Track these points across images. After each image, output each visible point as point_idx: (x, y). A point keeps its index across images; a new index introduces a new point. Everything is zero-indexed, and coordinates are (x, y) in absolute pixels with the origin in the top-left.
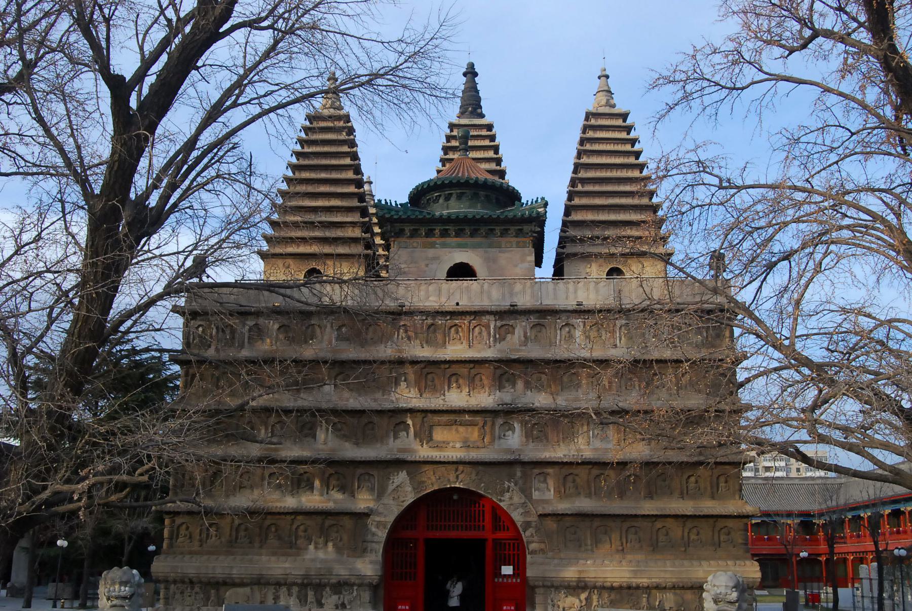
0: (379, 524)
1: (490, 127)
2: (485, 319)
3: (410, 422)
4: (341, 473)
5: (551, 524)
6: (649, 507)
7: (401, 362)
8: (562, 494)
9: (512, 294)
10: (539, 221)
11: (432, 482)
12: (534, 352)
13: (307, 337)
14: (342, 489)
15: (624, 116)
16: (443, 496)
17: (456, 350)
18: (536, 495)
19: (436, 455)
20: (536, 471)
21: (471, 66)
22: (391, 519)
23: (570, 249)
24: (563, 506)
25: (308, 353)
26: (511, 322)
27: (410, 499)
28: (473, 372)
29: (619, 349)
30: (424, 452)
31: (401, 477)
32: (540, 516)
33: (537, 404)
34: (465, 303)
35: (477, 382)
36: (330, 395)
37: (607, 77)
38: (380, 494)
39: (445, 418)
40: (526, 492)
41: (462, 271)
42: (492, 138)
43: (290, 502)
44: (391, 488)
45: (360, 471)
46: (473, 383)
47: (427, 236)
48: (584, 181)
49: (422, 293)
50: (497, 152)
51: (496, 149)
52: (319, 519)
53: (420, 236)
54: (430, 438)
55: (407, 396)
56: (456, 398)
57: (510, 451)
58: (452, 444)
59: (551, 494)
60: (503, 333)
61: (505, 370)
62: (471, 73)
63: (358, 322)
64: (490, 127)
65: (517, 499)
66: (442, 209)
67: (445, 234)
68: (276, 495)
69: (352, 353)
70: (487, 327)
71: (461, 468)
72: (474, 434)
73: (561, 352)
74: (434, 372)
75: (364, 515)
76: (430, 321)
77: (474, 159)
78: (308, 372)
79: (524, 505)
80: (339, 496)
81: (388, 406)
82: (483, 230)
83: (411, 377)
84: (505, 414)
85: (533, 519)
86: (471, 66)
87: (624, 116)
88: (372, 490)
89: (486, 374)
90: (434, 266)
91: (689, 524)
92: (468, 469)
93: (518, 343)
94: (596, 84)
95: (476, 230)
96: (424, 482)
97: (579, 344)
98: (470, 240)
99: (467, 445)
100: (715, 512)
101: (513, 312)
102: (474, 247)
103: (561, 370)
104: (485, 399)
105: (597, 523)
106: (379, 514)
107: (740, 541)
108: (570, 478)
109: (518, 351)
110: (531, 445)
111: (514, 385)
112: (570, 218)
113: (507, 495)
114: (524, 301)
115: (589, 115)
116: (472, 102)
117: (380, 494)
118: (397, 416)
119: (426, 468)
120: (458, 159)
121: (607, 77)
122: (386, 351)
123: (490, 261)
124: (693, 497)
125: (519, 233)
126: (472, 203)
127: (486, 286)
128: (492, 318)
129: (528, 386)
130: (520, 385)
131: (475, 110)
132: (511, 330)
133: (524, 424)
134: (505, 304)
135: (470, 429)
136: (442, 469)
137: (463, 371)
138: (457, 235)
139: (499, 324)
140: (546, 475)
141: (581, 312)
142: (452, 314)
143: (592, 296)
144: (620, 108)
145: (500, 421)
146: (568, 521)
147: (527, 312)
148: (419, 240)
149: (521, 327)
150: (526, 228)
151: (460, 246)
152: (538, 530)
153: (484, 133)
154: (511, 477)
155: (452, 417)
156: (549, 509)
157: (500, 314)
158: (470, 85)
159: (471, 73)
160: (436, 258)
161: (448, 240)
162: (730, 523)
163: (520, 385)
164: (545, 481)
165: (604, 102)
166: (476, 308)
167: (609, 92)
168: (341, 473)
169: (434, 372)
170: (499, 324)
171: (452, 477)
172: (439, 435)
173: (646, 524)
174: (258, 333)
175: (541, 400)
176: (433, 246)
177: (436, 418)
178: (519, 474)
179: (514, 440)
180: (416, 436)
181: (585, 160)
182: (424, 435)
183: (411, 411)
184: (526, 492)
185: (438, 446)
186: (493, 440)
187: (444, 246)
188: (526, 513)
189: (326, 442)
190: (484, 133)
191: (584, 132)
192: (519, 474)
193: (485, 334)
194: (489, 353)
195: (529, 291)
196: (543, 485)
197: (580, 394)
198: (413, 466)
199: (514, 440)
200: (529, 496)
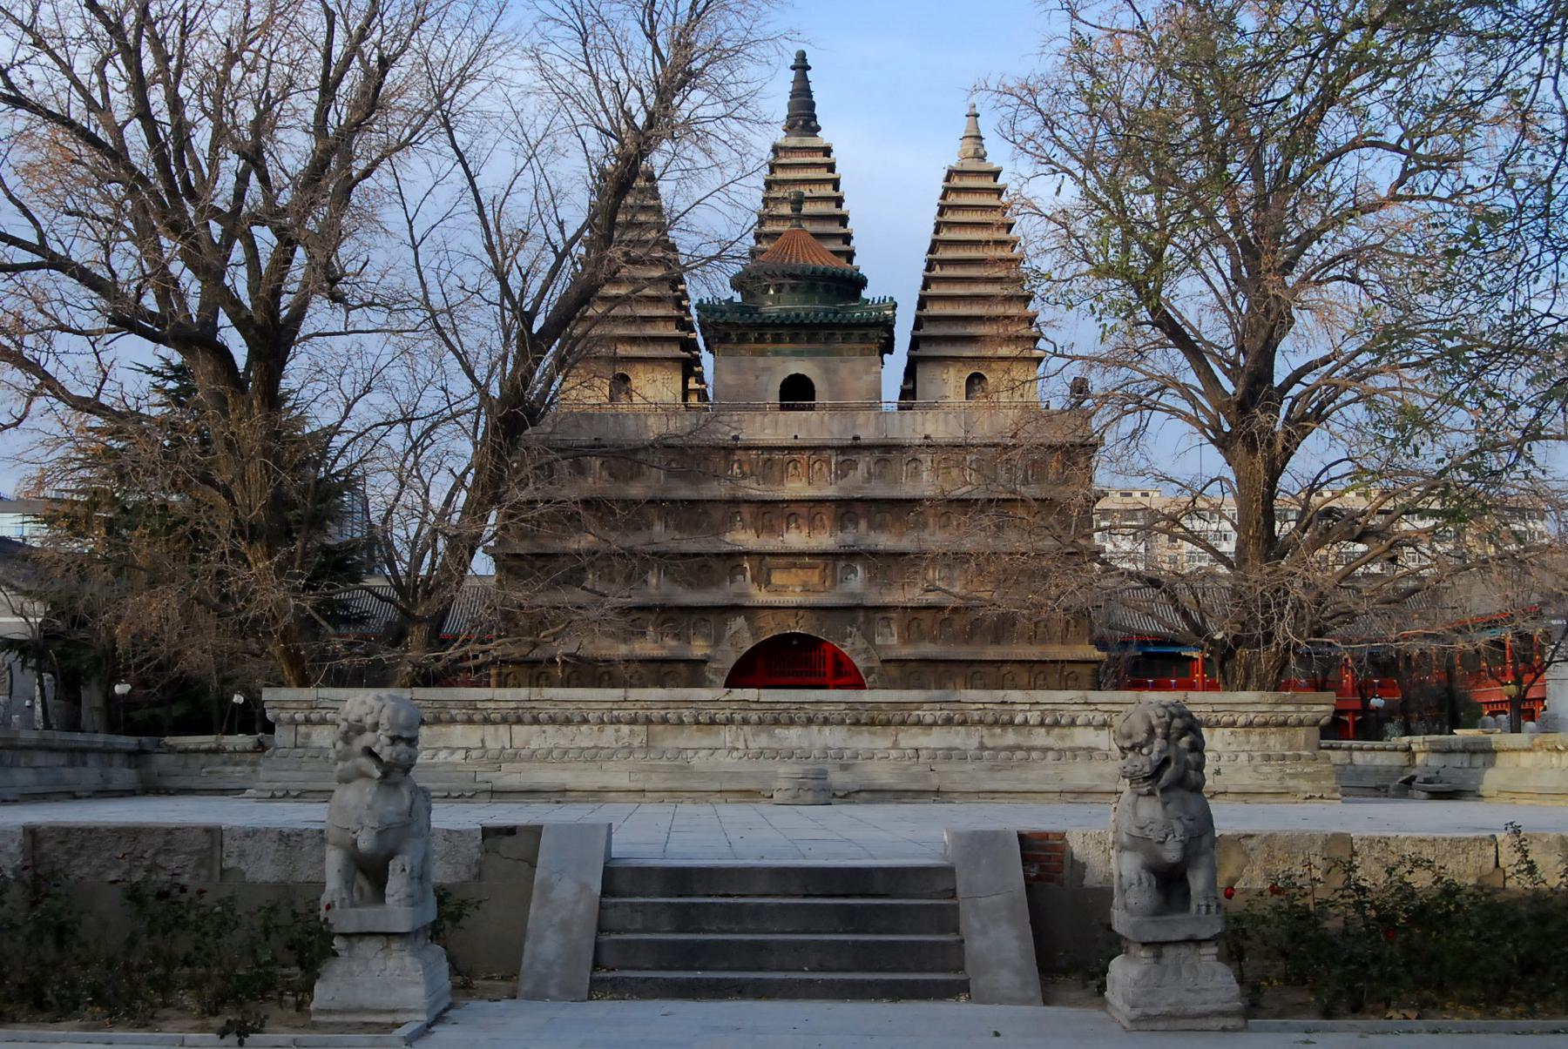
0: (717, 672)
1: (827, 151)
2: (826, 454)
3: (747, 565)
4: (672, 616)
5: (893, 670)
6: (992, 653)
7: (734, 502)
8: (906, 640)
9: (854, 426)
10: (888, 325)
11: (771, 628)
12: (879, 490)
13: (636, 475)
14: (677, 636)
15: (996, 174)
16: (783, 641)
17: (795, 488)
18: (878, 640)
19: (774, 599)
20: (879, 615)
21: (802, 56)
22: (730, 665)
23: (925, 350)
24: (907, 652)
25: (636, 490)
26: (854, 457)
27: (748, 645)
28: (814, 511)
29: (964, 484)
30: (761, 597)
31: (739, 622)
32: (884, 661)
33: (881, 547)
34: (804, 437)
35: (818, 522)
36: (662, 535)
37: (977, 116)
38: (717, 641)
39: (782, 561)
40: (868, 637)
41: (797, 392)
42: (831, 167)
43: (622, 650)
44: (728, 634)
45: (695, 617)
46: (812, 524)
47: (757, 341)
48: (943, 263)
49: (757, 425)
50: (836, 188)
51: (836, 184)
52: (653, 666)
53: (748, 341)
54: (768, 583)
55: (744, 538)
56: (796, 539)
57: (852, 595)
58: (791, 589)
59: (894, 640)
60: (845, 469)
61: (846, 509)
62: (801, 66)
63: (690, 456)
64: (827, 151)
65: (861, 644)
66: (772, 306)
67: (777, 339)
68: (607, 642)
69: (684, 492)
70: (829, 463)
71: (801, 613)
72: (814, 577)
73: (906, 490)
74: (771, 512)
75: (703, 662)
76: (766, 456)
77: (814, 235)
78: (638, 513)
79: (866, 651)
80: (671, 642)
81: (725, 549)
82: (822, 334)
83: (747, 517)
84: (848, 556)
85: (876, 664)
86: (802, 56)
87: (996, 174)
88: (707, 636)
89: (827, 515)
90: (765, 378)
91: (1036, 669)
92: (808, 614)
93: (860, 481)
94: (962, 126)
95: (814, 334)
96: (761, 628)
97: (925, 483)
98: (805, 347)
99: (806, 589)
100: (1061, 658)
101: (856, 447)
102: (812, 354)
103: (901, 509)
104: (825, 540)
105: (941, 668)
106: (716, 661)
107: (384, 316)
108: (915, 624)
109: (860, 488)
110: (874, 590)
111: (856, 524)
112: (921, 332)
113: (849, 640)
114: (868, 434)
115: (951, 174)
116: (803, 114)
117: (717, 641)
118: (733, 559)
119: (766, 612)
120: (789, 232)
121: (977, 116)
122: (717, 490)
123: (828, 372)
124: (1043, 642)
125: (864, 339)
126: (807, 296)
127: (826, 418)
128: (833, 453)
129: (872, 526)
130: (863, 525)
131: (807, 123)
132: (854, 465)
133: (868, 568)
134: (847, 439)
135: (809, 572)
136: (781, 615)
137: (803, 510)
138: (792, 341)
139: (841, 458)
140: (888, 620)
141: (930, 445)
142: (791, 449)
143: (941, 428)
144: (993, 161)
145: (842, 564)
146: (911, 667)
147: (870, 448)
148: (746, 346)
149: (864, 463)
150: (872, 333)
151: (795, 354)
152: (880, 675)
153: (819, 159)
154: (852, 622)
155: (791, 560)
156: (893, 654)
157: (841, 449)
158: (801, 85)
159: (801, 66)
160: (766, 369)
161: (781, 347)
162: (1078, 669)
163: (863, 525)
164: (888, 626)
165: (971, 153)
166: (816, 443)
167: (981, 138)
168: (672, 616)
169: (771, 512)
170: (841, 458)
171: (792, 624)
172: (778, 578)
173: (991, 669)
174: (580, 470)
175: (884, 541)
176: (763, 354)
177: (774, 561)
178: (861, 619)
179: (857, 584)
180: (753, 580)
181: (945, 235)
182: (763, 579)
183: (748, 554)
184: (868, 637)
185: (777, 590)
186: (834, 584)
187: (777, 353)
188: (869, 659)
189: (656, 588)
190: (819, 159)
191: (937, 232)
192: (861, 619)
193: (825, 469)
194: (830, 492)
195: (873, 422)
196: (886, 630)
197: (926, 535)
198: (750, 611)
199: (857, 584)
200: (871, 641)
